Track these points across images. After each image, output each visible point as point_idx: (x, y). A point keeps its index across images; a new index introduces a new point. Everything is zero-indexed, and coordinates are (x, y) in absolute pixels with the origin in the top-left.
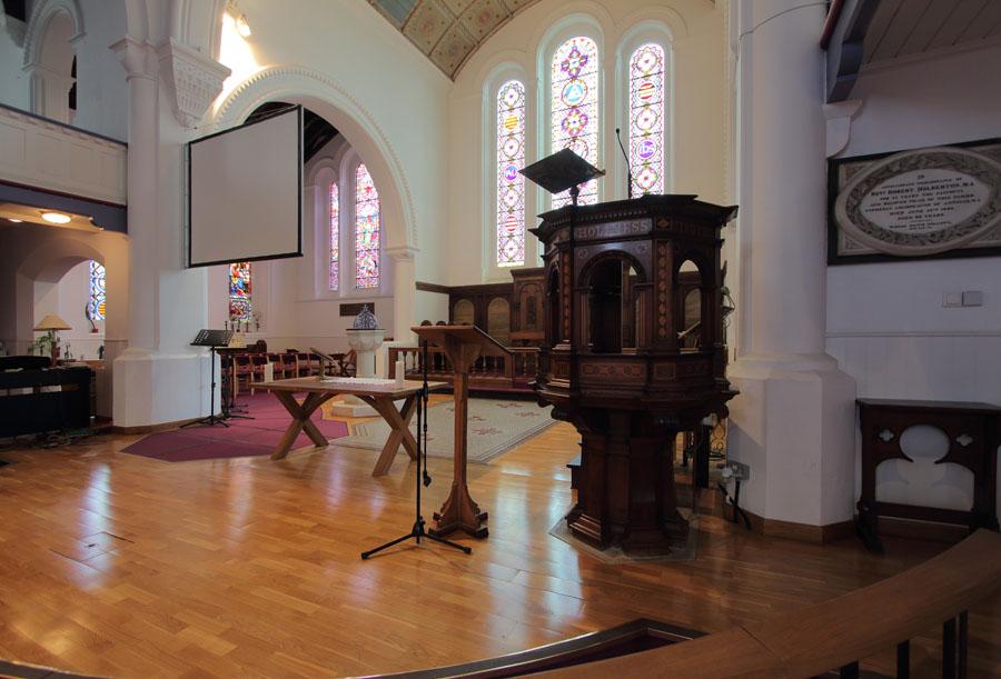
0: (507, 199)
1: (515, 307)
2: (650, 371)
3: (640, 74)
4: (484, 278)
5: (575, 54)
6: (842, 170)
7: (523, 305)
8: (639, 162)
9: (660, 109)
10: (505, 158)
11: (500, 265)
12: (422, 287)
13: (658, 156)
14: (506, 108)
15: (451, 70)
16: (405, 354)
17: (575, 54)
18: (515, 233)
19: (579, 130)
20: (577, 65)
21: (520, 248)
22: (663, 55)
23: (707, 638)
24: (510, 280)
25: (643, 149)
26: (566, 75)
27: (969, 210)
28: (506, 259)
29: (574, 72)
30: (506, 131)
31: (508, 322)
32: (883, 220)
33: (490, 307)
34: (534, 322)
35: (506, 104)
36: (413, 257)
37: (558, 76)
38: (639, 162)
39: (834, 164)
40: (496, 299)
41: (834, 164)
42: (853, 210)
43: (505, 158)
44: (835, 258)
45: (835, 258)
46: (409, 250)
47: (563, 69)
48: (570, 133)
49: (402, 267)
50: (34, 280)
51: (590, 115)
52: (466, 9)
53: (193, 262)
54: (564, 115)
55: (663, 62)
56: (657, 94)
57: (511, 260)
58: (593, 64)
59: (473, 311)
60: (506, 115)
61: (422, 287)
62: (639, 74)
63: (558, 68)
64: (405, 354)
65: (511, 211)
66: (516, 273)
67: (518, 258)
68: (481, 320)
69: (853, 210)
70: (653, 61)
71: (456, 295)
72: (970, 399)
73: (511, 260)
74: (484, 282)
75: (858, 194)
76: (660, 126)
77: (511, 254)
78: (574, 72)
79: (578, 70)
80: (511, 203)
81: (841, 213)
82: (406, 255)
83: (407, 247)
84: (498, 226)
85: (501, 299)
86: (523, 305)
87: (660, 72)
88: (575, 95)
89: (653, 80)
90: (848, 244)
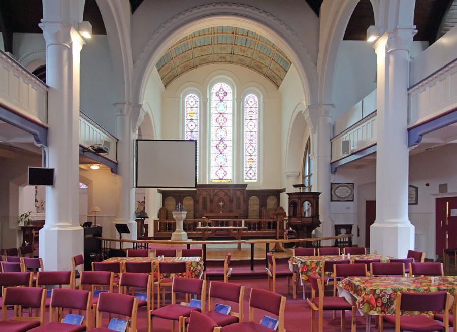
1: (196, 202)
2: (313, 220)
3: (248, 106)
5: (222, 90)
6: (333, 185)
7: (201, 201)
8: (248, 143)
9: (256, 122)
10: (188, 130)
13: (255, 142)
14: (189, 106)
15: (165, 84)
17: (222, 90)
19: (223, 124)
20: (223, 95)
22: (257, 100)
23: (450, 31)
25: (250, 137)
26: (217, 99)
27: (348, 194)
29: (221, 98)
30: (189, 118)
32: (338, 194)
35: (189, 104)
37: (214, 98)
38: (248, 143)
39: (332, 184)
40: (168, 198)
41: (332, 184)
42: (334, 192)
43: (188, 130)
44: (332, 200)
45: (332, 200)
47: (216, 95)
48: (220, 124)
50: (19, 186)
52: (182, 64)
53: (138, 186)
54: (217, 116)
55: (257, 103)
56: (255, 116)
58: (230, 97)
60: (189, 110)
62: (248, 106)
63: (214, 95)
69: (334, 192)
70: (253, 102)
75: (335, 190)
76: (256, 129)
78: (221, 98)
79: (223, 98)
81: (333, 193)
85: (189, 197)
86: (201, 201)
87: (256, 108)
88: (221, 159)
89: (253, 109)
90: (334, 198)
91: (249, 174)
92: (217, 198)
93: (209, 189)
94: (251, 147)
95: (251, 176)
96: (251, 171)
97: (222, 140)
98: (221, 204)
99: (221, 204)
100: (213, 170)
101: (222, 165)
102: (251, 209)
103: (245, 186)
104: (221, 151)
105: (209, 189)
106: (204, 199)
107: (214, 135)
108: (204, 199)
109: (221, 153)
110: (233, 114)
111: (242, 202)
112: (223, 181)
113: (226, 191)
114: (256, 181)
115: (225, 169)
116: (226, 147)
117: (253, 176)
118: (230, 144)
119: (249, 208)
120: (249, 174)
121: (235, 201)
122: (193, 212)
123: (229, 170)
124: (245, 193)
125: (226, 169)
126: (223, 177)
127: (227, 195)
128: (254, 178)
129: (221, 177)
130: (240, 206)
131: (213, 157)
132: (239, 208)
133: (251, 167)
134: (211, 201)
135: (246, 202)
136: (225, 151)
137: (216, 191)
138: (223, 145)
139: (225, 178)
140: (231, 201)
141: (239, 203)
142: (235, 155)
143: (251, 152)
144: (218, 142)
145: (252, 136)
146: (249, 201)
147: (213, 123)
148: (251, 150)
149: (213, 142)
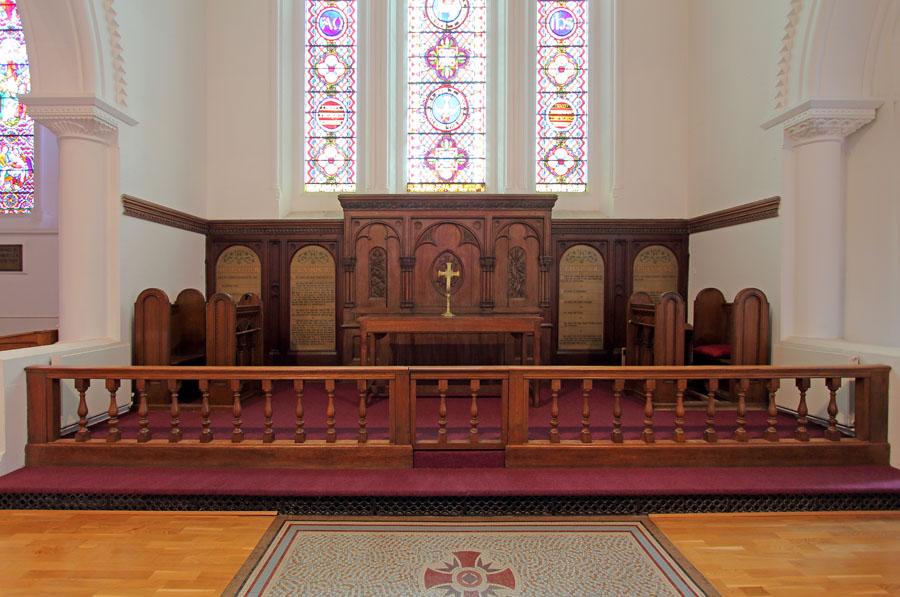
0: (322, 69)
4: (282, 208)
7: (363, 263)
11: (310, 188)
12: (135, 208)
16: (83, 386)
18: (340, 132)
21: (348, 160)
24: (337, 213)
28: (320, 178)
31: (331, 290)
33: (294, 263)
34: (383, 293)
36: (113, 133)
46: (97, 112)
49: (80, 153)
51: (472, 152)
57: (331, 181)
59: (258, 270)
61: (135, 208)
64: (83, 386)
65: (331, 92)
66: (346, 201)
67: (343, 178)
68: (276, 287)
71: (220, 237)
72: (762, 199)
73: (331, 181)
74: (281, 214)
77: (331, 169)
80: (331, 78)
82: (91, 125)
83: (92, 101)
84: (307, 117)
86: (363, 263)
88: (447, 107)
91: (552, 164)
92: (428, 254)
93: (397, 214)
94: (562, 61)
95: (561, 170)
96: (561, 153)
97: (447, 31)
98: (449, 274)
99: (449, 274)
100: (416, 147)
101: (452, 126)
102: (574, 296)
103: (549, 201)
104: (447, 73)
105: (397, 214)
106: (378, 257)
107: (418, 13)
108: (378, 257)
109: (446, 84)
110: (492, 34)
111: (532, 267)
112: (453, 189)
113: (468, 223)
114: (581, 189)
115: (460, 44)
116: (465, 56)
117: (572, 79)
118: (478, 46)
119: (561, 291)
120: (552, 164)
121: (503, 263)
122: (333, 305)
123: (478, 147)
124: (548, 231)
125: (463, 142)
126: (455, 174)
127: (469, 238)
128: (574, 178)
129: (447, 175)
130: (523, 283)
131: (415, 98)
132: (521, 293)
133: (561, 139)
134: (407, 264)
135: (550, 265)
136: (462, 75)
137: (426, 224)
138: (453, 52)
139: (462, 176)
140: (488, 264)
141: (521, 270)
142: (500, 156)
143: (562, 78)
144: (433, 40)
145: (567, 15)
146: (563, 263)
147: (416, 69)
148: (561, 69)
149: (415, 41)
